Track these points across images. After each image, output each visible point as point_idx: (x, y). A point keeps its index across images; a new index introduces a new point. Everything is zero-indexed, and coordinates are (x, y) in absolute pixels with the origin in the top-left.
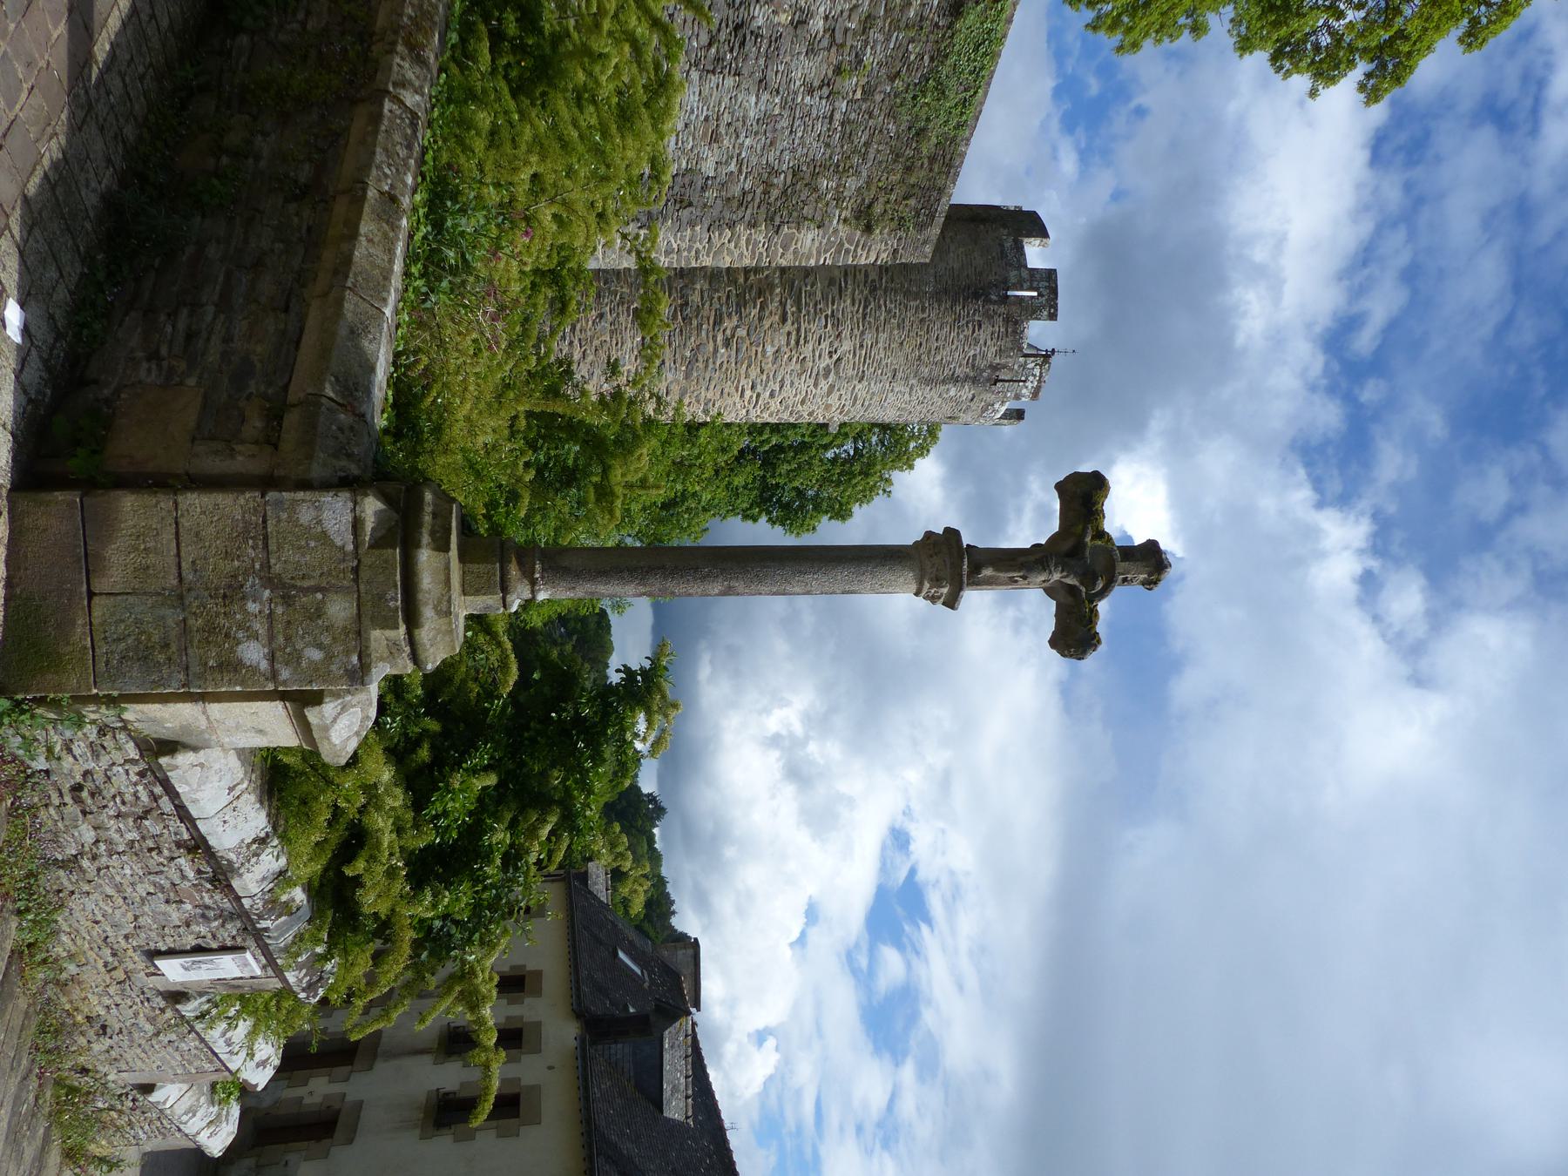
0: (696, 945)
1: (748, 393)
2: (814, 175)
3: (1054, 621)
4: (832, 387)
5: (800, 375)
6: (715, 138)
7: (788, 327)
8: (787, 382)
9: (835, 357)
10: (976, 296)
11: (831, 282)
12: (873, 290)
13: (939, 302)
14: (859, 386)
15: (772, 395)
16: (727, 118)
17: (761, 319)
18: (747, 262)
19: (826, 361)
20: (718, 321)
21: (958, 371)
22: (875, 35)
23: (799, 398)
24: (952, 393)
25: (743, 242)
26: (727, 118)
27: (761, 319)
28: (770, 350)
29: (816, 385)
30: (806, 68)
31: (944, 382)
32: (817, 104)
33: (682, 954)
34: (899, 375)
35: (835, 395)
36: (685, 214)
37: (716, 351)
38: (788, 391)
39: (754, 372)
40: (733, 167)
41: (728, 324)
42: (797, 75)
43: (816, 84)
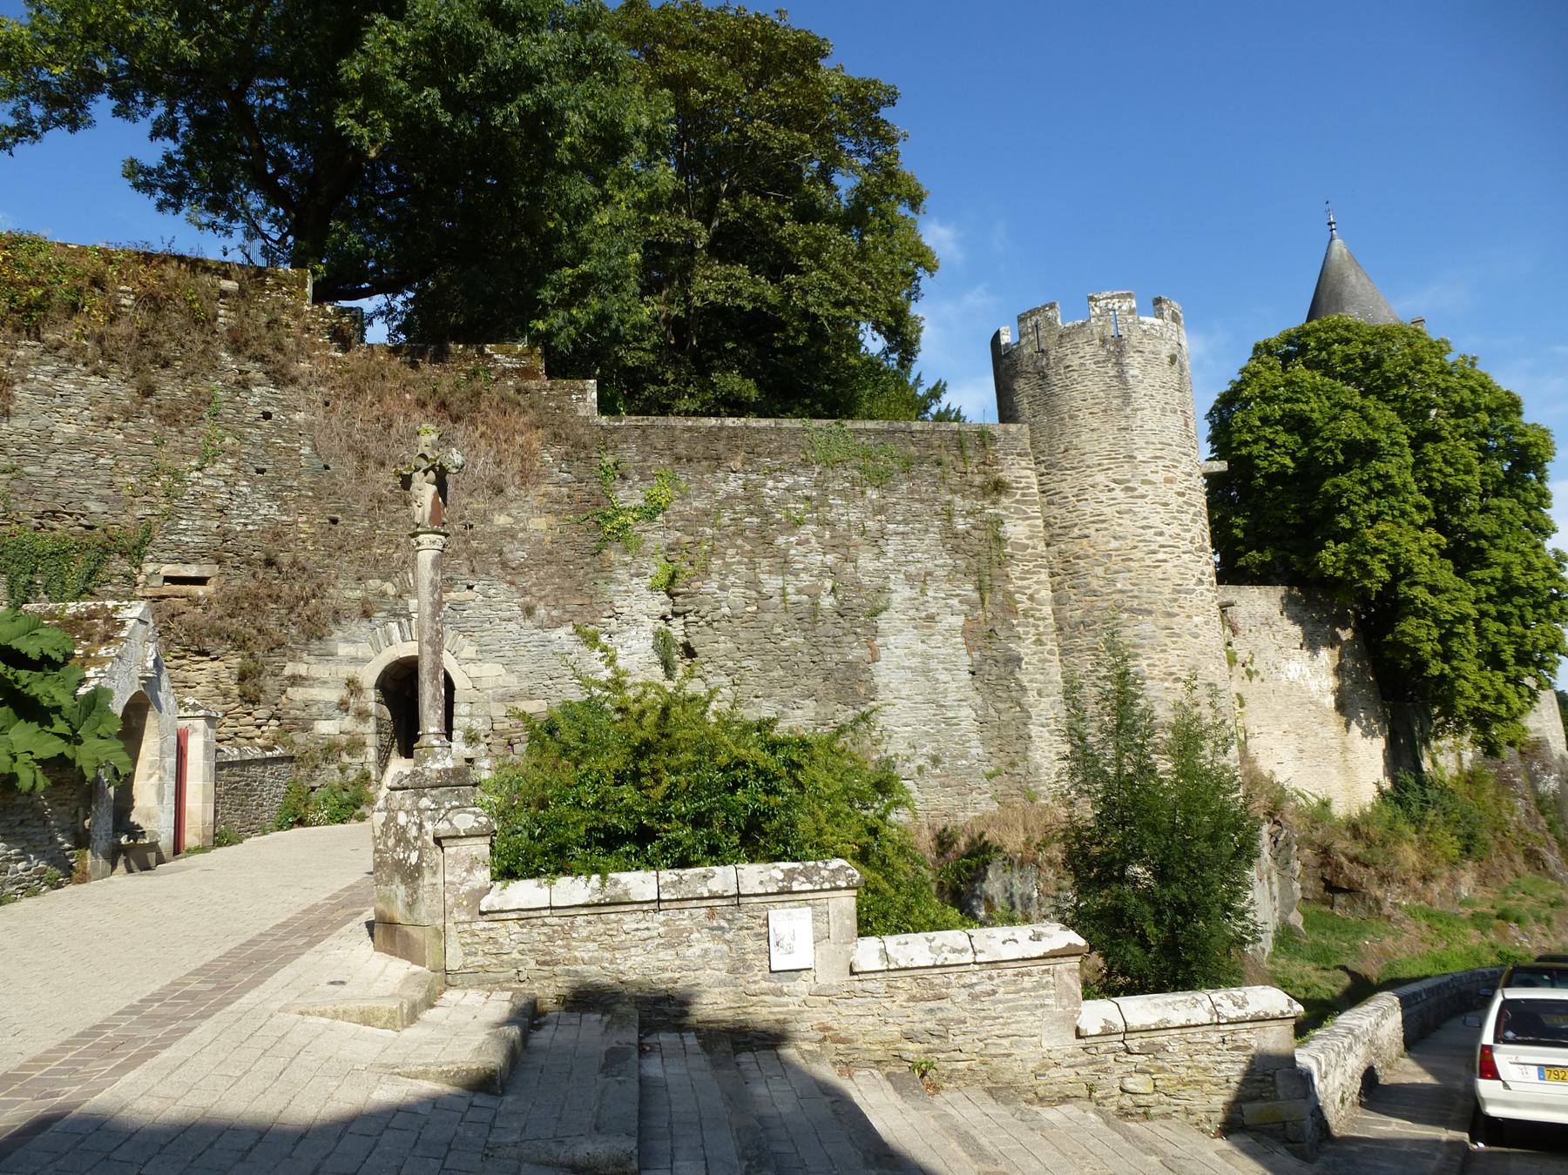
0: (377, 686)
1: (1161, 556)
2: (956, 536)
3: (134, 792)
4: (1144, 482)
5: (1135, 513)
6: (931, 618)
7: (1092, 532)
8: (1144, 523)
9: (1113, 485)
10: (1044, 377)
11: (1051, 503)
12: (1052, 466)
13: (1054, 407)
14: (1140, 458)
15: (1161, 534)
16: (912, 613)
17: (1088, 557)
18: (1044, 576)
19: (1119, 493)
20: (1095, 593)
21: (1112, 373)
22: (831, 516)
23: (1160, 508)
24: (1135, 372)
25: (1025, 583)
26: (912, 613)
27: (1088, 557)
28: (1114, 544)
29: (1143, 497)
30: (866, 561)
31: (1125, 383)
32: (892, 547)
33: (389, 686)
34: (1123, 423)
35: (1152, 477)
36: (1002, 635)
37: (1121, 591)
38: (1155, 520)
39: (1137, 554)
40: (955, 602)
41: (1095, 584)
42: (871, 566)
43: (876, 550)
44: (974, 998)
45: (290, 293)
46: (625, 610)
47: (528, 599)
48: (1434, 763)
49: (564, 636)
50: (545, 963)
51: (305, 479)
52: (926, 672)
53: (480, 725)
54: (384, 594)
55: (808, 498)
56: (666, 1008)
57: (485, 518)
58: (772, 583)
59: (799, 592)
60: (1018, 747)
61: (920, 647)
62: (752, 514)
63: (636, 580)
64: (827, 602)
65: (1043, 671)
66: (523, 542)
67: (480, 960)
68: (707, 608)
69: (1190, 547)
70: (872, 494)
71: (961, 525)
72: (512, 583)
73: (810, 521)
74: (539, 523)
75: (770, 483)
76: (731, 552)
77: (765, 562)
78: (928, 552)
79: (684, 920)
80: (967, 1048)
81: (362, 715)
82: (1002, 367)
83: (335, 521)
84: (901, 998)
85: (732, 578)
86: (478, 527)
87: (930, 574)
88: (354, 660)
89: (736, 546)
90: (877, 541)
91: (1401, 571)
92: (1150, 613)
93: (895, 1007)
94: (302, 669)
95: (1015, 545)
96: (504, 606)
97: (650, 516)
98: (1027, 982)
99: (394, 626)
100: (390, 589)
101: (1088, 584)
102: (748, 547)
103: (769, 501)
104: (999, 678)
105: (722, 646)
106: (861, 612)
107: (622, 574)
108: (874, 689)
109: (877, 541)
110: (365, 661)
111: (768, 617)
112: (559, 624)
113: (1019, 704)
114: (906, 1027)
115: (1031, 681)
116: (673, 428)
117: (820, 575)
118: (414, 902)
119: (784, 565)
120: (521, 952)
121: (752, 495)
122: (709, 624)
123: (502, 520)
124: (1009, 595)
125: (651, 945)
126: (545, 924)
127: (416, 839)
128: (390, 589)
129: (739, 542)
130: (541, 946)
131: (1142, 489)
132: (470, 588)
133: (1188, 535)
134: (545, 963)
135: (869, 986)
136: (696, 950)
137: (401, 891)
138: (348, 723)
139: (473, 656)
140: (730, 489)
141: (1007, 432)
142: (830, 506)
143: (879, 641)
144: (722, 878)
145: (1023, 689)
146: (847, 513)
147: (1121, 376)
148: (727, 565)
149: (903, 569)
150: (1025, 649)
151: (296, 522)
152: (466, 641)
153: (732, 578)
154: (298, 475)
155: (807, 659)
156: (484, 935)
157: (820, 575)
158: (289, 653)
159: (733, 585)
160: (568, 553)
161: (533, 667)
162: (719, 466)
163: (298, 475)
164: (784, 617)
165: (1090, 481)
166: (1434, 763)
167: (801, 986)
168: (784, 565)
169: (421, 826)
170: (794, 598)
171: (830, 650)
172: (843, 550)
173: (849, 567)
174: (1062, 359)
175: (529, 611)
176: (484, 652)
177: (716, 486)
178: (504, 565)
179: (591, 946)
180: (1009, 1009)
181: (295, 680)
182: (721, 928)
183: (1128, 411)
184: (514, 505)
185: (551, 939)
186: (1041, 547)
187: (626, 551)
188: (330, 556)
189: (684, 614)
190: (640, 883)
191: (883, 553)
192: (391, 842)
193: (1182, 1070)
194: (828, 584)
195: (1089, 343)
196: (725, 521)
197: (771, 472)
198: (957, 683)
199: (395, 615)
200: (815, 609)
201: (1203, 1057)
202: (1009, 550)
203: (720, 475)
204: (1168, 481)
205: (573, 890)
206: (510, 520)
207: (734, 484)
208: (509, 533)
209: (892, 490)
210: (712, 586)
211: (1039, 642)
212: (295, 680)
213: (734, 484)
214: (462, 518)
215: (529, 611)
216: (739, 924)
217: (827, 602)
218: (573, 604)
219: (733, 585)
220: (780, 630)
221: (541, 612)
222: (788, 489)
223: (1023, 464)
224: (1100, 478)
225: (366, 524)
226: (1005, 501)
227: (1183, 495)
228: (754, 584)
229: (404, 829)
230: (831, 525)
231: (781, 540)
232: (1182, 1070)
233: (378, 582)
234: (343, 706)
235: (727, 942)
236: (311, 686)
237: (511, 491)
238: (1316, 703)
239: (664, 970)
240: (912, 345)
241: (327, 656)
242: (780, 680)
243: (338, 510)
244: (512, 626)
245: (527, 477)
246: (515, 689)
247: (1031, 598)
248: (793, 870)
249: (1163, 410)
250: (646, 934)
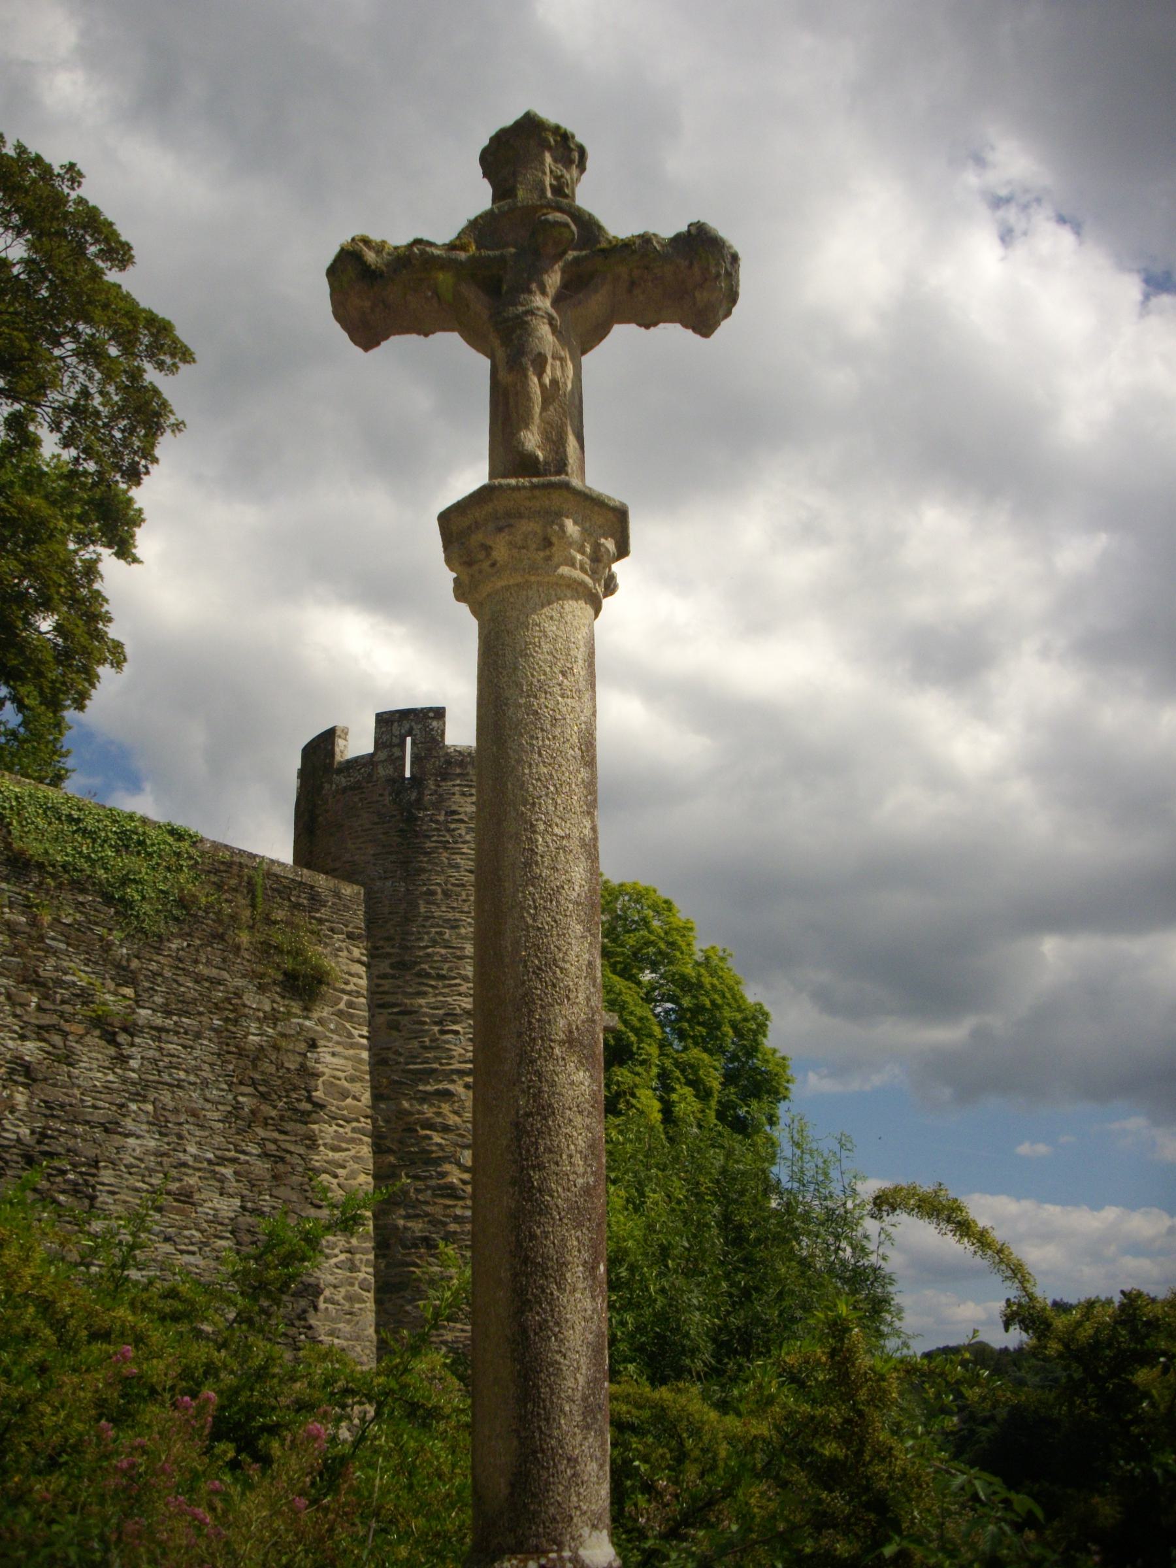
2: (241, 1053)
10: (412, 819)
11: (394, 1026)
25: (337, 1156)
32: (140, 1052)
40: (228, 1171)
43: (112, 1051)
97: (740, 1401)
101: (443, 1175)
115: (331, 1333)
141: (337, 894)
172: (57, 1039)
223: (356, 952)
240: (158, 415)
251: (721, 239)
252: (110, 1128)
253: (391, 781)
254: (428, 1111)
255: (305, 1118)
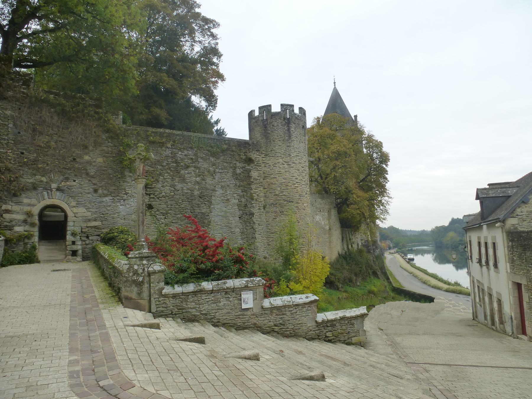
1: (296, 185)
2: (237, 174)
4: (293, 163)
6: (228, 200)
10: (266, 127)
12: (266, 155)
15: (297, 179)
19: (286, 166)
22: (199, 165)
24: (293, 129)
28: (284, 181)
29: (293, 167)
30: (209, 180)
31: (290, 132)
34: (288, 145)
36: (249, 206)
37: (284, 195)
38: (295, 175)
39: (290, 184)
40: (235, 195)
43: (212, 177)
44: (292, 314)
45: (5, 65)
46: (130, 192)
47: (95, 186)
48: (352, 246)
49: (108, 200)
50: (180, 309)
51: (11, 136)
52: (226, 217)
53: (78, 230)
54: (42, 181)
55: (192, 159)
56: (214, 320)
57: (81, 157)
58: (179, 186)
59: (188, 189)
60: (252, 241)
61: (225, 209)
62: (173, 162)
63: (134, 182)
64: (196, 193)
65: (260, 218)
66: (94, 166)
67: (161, 309)
68: (158, 193)
69: (304, 183)
70: (212, 159)
71: (238, 171)
72: (90, 180)
73: (192, 166)
74: (100, 160)
75: (180, 153)
76: (166, 175)
77: (177, 179)
78: (228, 178)
79: (219, 296)
80: (290, 327)
81: (33, 225)
82: (252, 122)
83: (22, 153)
84: (274, 315)
85: (166, 183)
86: (78, 160)
87: (228, 186)
88: (29, 205)
89: (168, 173)
90: (212, 174)
91: (349, 191)
92: (293, 202)
93: (272, 318)
94: (9, 207)
95: (254, 179)
96: (87, 188)
98: (304, 309)
99: (45, 193)
100: (44, 179)
102: (172, 174)
103: (179, 159)
104: (247, 219)
105: (162, 206)
106: (205, 197)
107: (129, 179)
108: (210, 222)
109: (212, 174)
110: (34, 205)
111: (178, 197)
112: (106, 196)
113: (253, 228)
114: (275, 323)
116: (148, 131)
117: (194, 185)
118: (141, 292)
119: (183, 180)
120: (173, 306)
121: (174, 156)
122: (158, 198)
123: (87, 158)
124: (251, 194)
125: (209, 303)
126: (180, 298)
127: (142, 273)
128: (44, 179)
129: (169, 171)
130: (179, 304)
131: (293, 165)
132: (74, 181)
133: (304, 180)
134: (180, 309)
135: (266, 312)
136: (222, 304)
137: (135, 289)
138: (27, 228)
139: (75, 205)
140: (166, 154)
142: (199, 162)
143: (212, 206)
144: (231, 283)
145: (254, 223)
146: (204, 165)
147: (289, 130)
148: (165, 179)
149: (220, 184)
150: (255, 211)
151: (7, 152)
152: (72, 200)
153: (166, 183)
154: (7, 134)
155: (189, 211)
156: (162, 302)
157: (194, 185)
158: (4, 201)
159: (166, 186)
160: (110, 171)
161: (96, 210)
162: (163, 146)
163: (7, 134)
164: (182, 197)
165: (278, 161)
166: (352, 246)
167: (249, 313)
168: (183, 180)
169: (144, 270)
170: (186, 191)
171: (197, 209)
173: (204, 182)
174: (272, 123)
175: (96, 191)
176: (79, 204)
177: (162, 152)
178: (87, 174)
179: (193, 304)
180: (300, 317)
181: (7, 211)
182: (229, 297)
183: (290, 141)
184: (92, 153)
185: (182, 302)
186: (262, 180)
187: (130, 172)
188: (21, 166)
189: (150, 195)
190: (207, 285)
191: (214, 178)
192: (131, 274)
193: (339, 330)
194: (197, 187)
195: (280, 119)
196: (165, 164)
197: (180, 150)
198: (235, 221)
199: (46, 189)
200: (192, 195)
201: (344, 327)
202: (252, 180)
203: (164, 148)
204: (300, 163)
205: (190, 287)
206: (90, 158)
207: (168, 152)
208: (89, 163)
209: (218, 158)
210: (159, 186)
211: (259, 209)
212: (7, 211)
213: (168, 152)
214: (72, 156)
215: (96, 191)
216: (233, 296)
217: (196, 193)
218: (112, 189)
219: (166, 186)
220: (181, 201)
221: (100, 191)
222: (185, 155)
224: (281, 160)
225: (35, 155)
226: (252, 165)
227: (303, 167)
228: (173, 186)
229: (136, 270)
230: (199, 168)
231: (182, 172)
232: (339, 330)
233: (40, 177)
234: (25, 221)
235: (230, 301)
236: (12, 214)
237: (91, 148)
238: (323, 228)
239: (213, 310)
241: (19, 203)
242: (181, 218)
243: (24, 149)
244: (89, 196)
245: (96, 144)
246: (90, 218)
247: (258, 195)
248: (248, 281)
249: (300, 142)
250: (208, 300)
251: (422, 231)
252: (214, 190)
253: (262, 120)
254: (272, 181)
255: (249, 184)
